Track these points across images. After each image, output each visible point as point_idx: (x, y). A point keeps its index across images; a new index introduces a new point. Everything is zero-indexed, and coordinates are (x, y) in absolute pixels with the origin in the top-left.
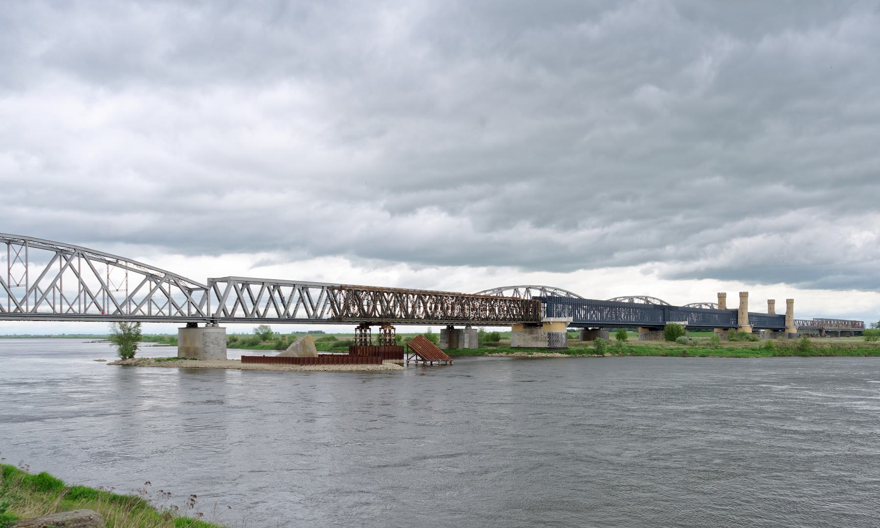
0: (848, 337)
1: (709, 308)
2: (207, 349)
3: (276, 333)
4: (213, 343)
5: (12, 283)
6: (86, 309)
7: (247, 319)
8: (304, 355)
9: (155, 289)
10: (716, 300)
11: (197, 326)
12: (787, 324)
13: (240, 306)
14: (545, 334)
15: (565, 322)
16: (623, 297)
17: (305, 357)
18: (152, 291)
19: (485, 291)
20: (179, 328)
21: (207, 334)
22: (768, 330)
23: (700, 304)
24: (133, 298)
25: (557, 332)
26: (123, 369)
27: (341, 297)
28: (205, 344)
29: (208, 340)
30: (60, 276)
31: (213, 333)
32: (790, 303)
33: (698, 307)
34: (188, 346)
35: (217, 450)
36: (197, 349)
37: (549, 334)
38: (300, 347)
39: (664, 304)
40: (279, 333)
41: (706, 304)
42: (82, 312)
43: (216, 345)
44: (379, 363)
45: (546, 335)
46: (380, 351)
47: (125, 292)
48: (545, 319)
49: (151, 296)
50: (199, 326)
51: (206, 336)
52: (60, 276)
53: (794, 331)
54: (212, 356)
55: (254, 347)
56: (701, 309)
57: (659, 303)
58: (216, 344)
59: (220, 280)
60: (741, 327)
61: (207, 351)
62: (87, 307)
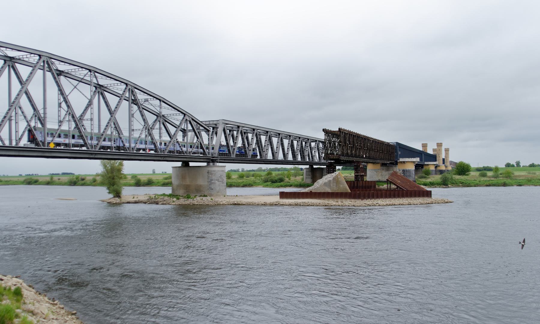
0: (282, 168)
2: (212, 186)
4: (218, 180)
6: (17, 144)
8: (338, 190)
11: (183, 163)
14: (400, 170)
17: (339, 191)
20: (173, 167)
21: (213, 172)
25: (410, 169)
26: (110, 208)
28: (210, 182)
29: (214, 178)
31: (218, 171)
34: (187, 184)
35: (230, 282)
36: (201, 186)
37: (404, 171)
38: (333, 182)
39: (59, 93)
42: (14, 144)
43: (221, 183)
44: (429, 196)
45: (401, 171)
46: (359, 185)
47: (158, 130)
50: (190, 165)
51: (211, 174)
54: (218, 192)
55: (168, 186)
58: (220, 181)
61: (212, 188)
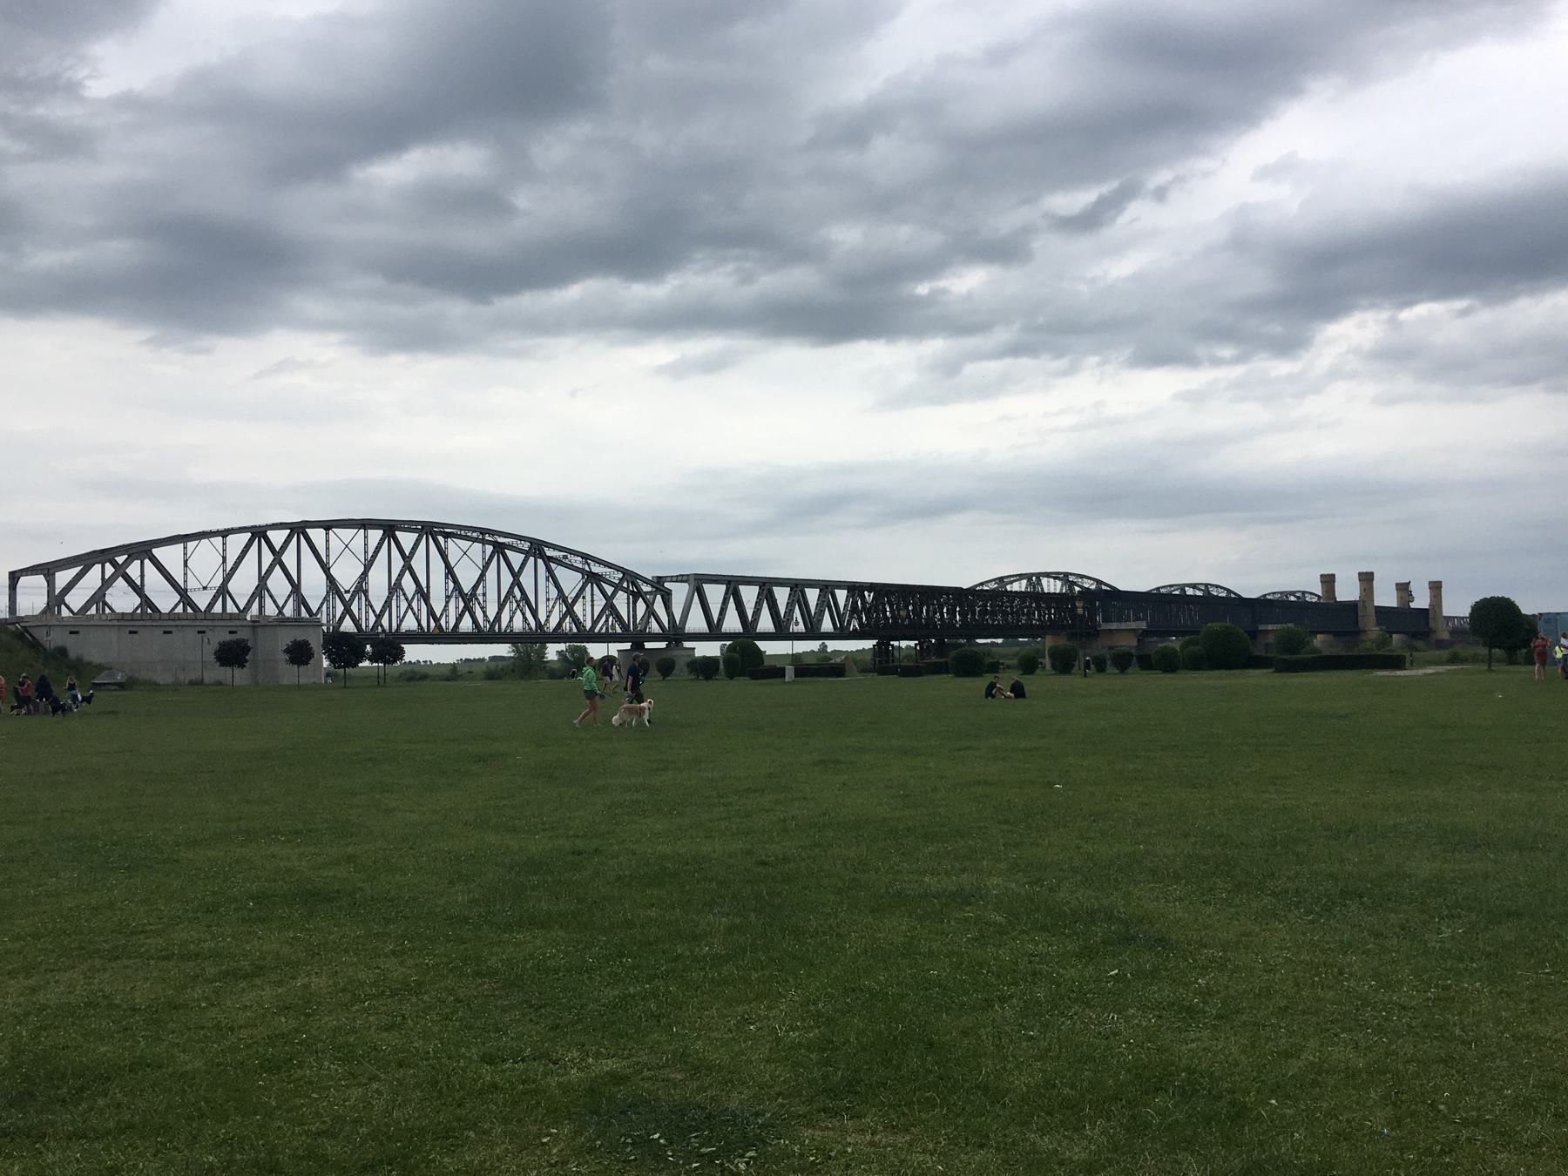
1: (1199, 593)
3: (426, 662)
5: (192, 584)
7: (478, 637)
9: (113, 578)
10: (1318, 589)
12: (1431, 625)
13: (106, 608)
15: (1134, 630)
16: (1018, 575)
18: (107, 583)
19: (982, 584)
20: (618, 651)
22: (1399, 635)
23: (1182, 587)
24: (67, 599)
27: (869, 596)
30: (88, 562)
32: (1436, 587)
33: (1177, 592)
37: (1266, 644)
40: (430, 662)
41: (1194, 586)
48: (1105, 626)
49: (104, 595)
52: (88, 562)
53: (1445, 636)
56: (1184, 594)
57: (1224, 595)
59: (674, 579)
60: (1366, 631)
62: (715, 618)
